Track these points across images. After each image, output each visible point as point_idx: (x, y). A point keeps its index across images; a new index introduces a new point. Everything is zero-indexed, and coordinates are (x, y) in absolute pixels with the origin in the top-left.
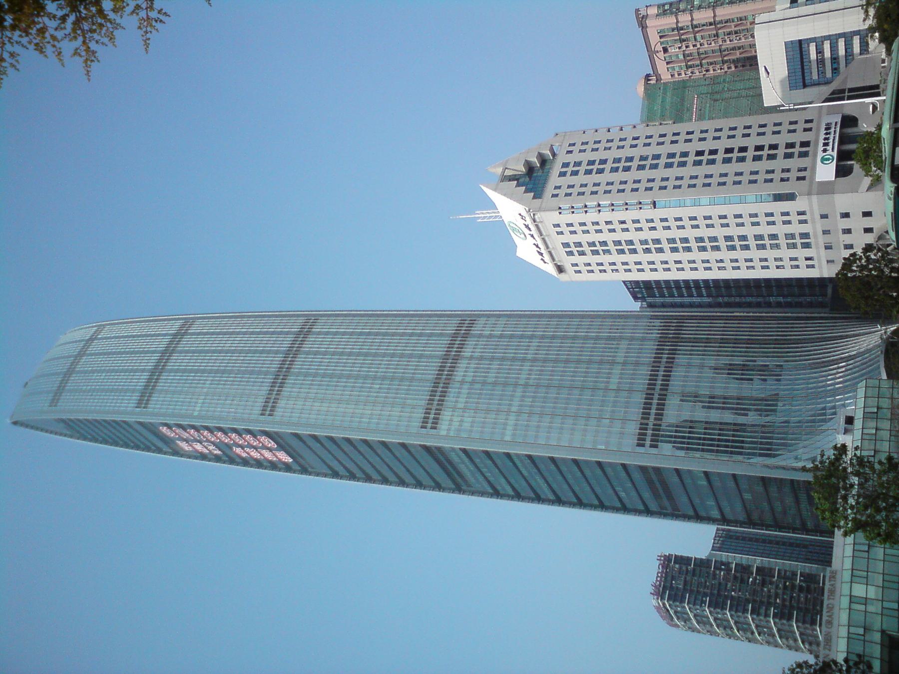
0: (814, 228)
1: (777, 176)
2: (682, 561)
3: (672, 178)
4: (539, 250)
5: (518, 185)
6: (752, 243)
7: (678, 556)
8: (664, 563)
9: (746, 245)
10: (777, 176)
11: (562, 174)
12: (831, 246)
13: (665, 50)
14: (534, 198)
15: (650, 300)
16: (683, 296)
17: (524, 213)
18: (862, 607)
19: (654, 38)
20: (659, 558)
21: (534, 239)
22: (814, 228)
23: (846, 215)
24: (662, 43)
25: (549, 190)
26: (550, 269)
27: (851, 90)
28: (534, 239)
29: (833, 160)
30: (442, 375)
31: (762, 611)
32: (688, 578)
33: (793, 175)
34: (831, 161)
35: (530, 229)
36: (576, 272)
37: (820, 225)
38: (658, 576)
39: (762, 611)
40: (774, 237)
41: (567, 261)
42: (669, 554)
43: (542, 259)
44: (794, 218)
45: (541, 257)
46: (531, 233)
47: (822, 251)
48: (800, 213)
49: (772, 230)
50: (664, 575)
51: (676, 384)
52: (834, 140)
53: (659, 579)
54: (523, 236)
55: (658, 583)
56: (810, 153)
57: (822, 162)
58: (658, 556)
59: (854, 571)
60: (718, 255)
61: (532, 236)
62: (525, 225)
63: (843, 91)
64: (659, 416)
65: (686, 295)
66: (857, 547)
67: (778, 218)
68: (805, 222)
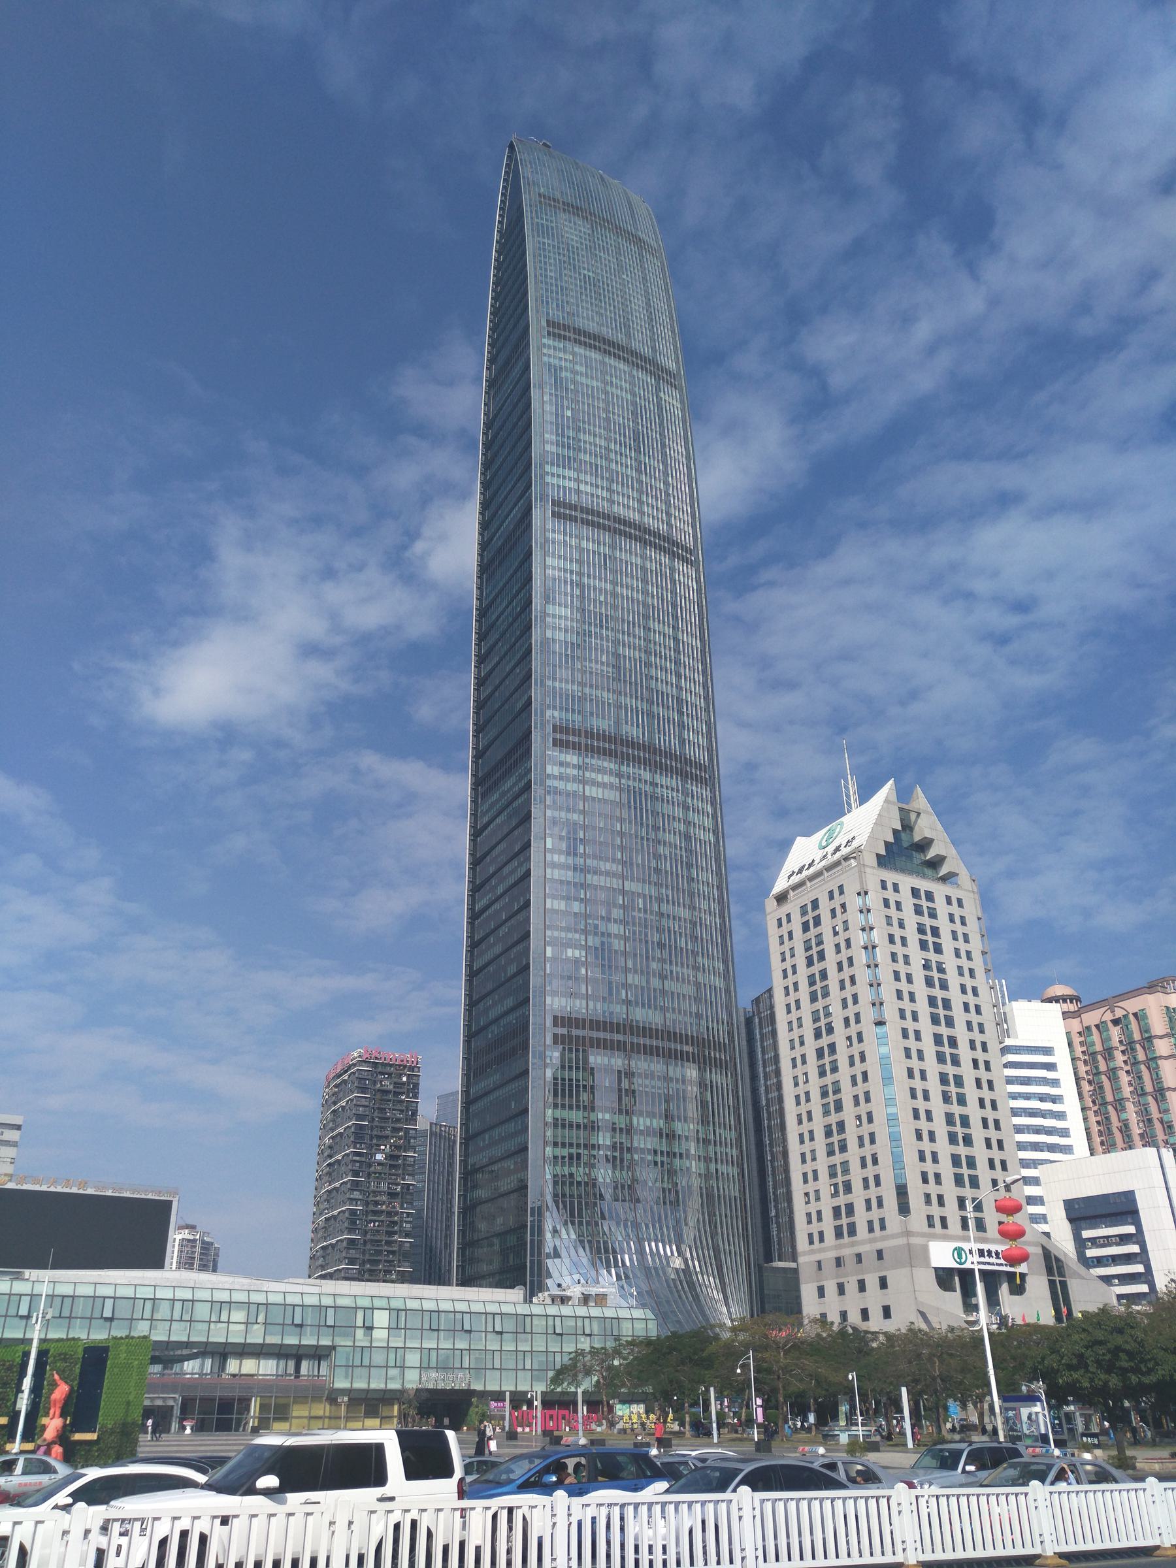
0: (863, 1242)
1: (932, 1189)
3: (911, 988)
5: (895, 832)
10: (932, 1189)
11: (915, 892)
13: (1116, 1022)
14: (878, 856)
17: (855, 844)
18: (360, 1323)
19: (1132, 1005)
21: (821, 860)
22: (863, 1242)
23: (883, 1283)
24: (1125, 1016)
25: (891, 877)
26: (780, 885)
27: (1064, 1285)
28: (821, 860)
29: (960, 1263)
30: (628, 746)
31: (356, 1195)
32: (390, 1096)
33: (936, 1211)
35: (835, 853)
36: (779, 920)
37: (867, 1249)
39: (356, 1195)
40: (848, 1188)
41: (792, 907)
43: (793, 873)
44: (875, 1214)
45: (796, 871)
46: (829, 856)
47: (832, 1254)
48: (882, 1221)
49: (857, 1185)
51: (640, 1064)
52: (989, 1264)
54: (824, 844)
56: (931, 1230)
57: (955, 1249)
59: (404, 1313)
61: (825, 857)
62: (840, 846)
63: (1061, 1274)
64: (598, 1044)
66: (435, 1315)
67: (873, 1193)
68: (871, 1230)
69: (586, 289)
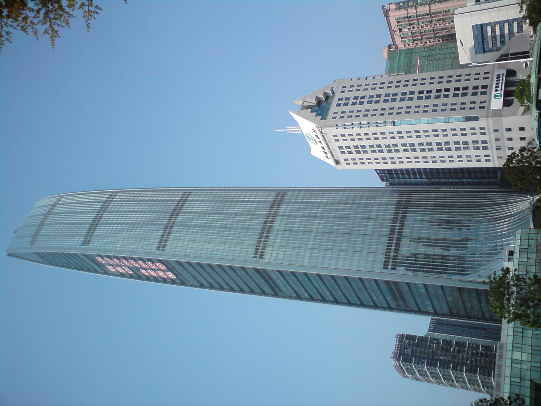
0: (490, 138)
1: (467, 106)
2: (411, 338)
3: (404, 107)
4: (324, 151)
5: (312, 112)
6: (453, 146)
7: (408, 335)
8: (400, 339)
9: (449, 148)
10: (467, 106)
11: (338, 105)
12: (500, 148)
13: (400, 30)
14: (321, 119)
15: (391, 181)
16: (411, 178)
17: (315, 129)
18: (519, 366)
20: (397, 336)
21: (321, 144)
22: (490, 138)
23: (509, 130)
24: (398, 26)
25: (331, 114)
26: (331, 162)
27: (512, 54)
28: (321, 144)
29: (501, 96)
30: (266, 226)
33: (477, 105)
34: (500, 97)
35: (319, 138)
36: (347, 164)
37: (493, 136)
38: (396, 347)
39: (459, 368)
40: (466, 143)
41: (341, 157)
42: (403, 334)
43: (326, 156)
44: (478, 131)
45: (326, 155)
46: (320, 140)
47: (495, 151)
48: (481, 129)
49: (465, 138)
50: (399, 346)
51: (407, 231)
52: (502, 84)
53: (396, 349)
54: (314, 142)
55: (396, 351)
56: (488, 92)
57: (495, 98)
58: (396, 335)
59: (514, 344)
60: (432, 154)
61: (320, 142)
62: (316, 135)
63: (507, 55)
64: (397, 251)
65: (413, 178)
66: (516, 330)
67: (468, 131)
68: (485, 134)
69: (62, 240)
